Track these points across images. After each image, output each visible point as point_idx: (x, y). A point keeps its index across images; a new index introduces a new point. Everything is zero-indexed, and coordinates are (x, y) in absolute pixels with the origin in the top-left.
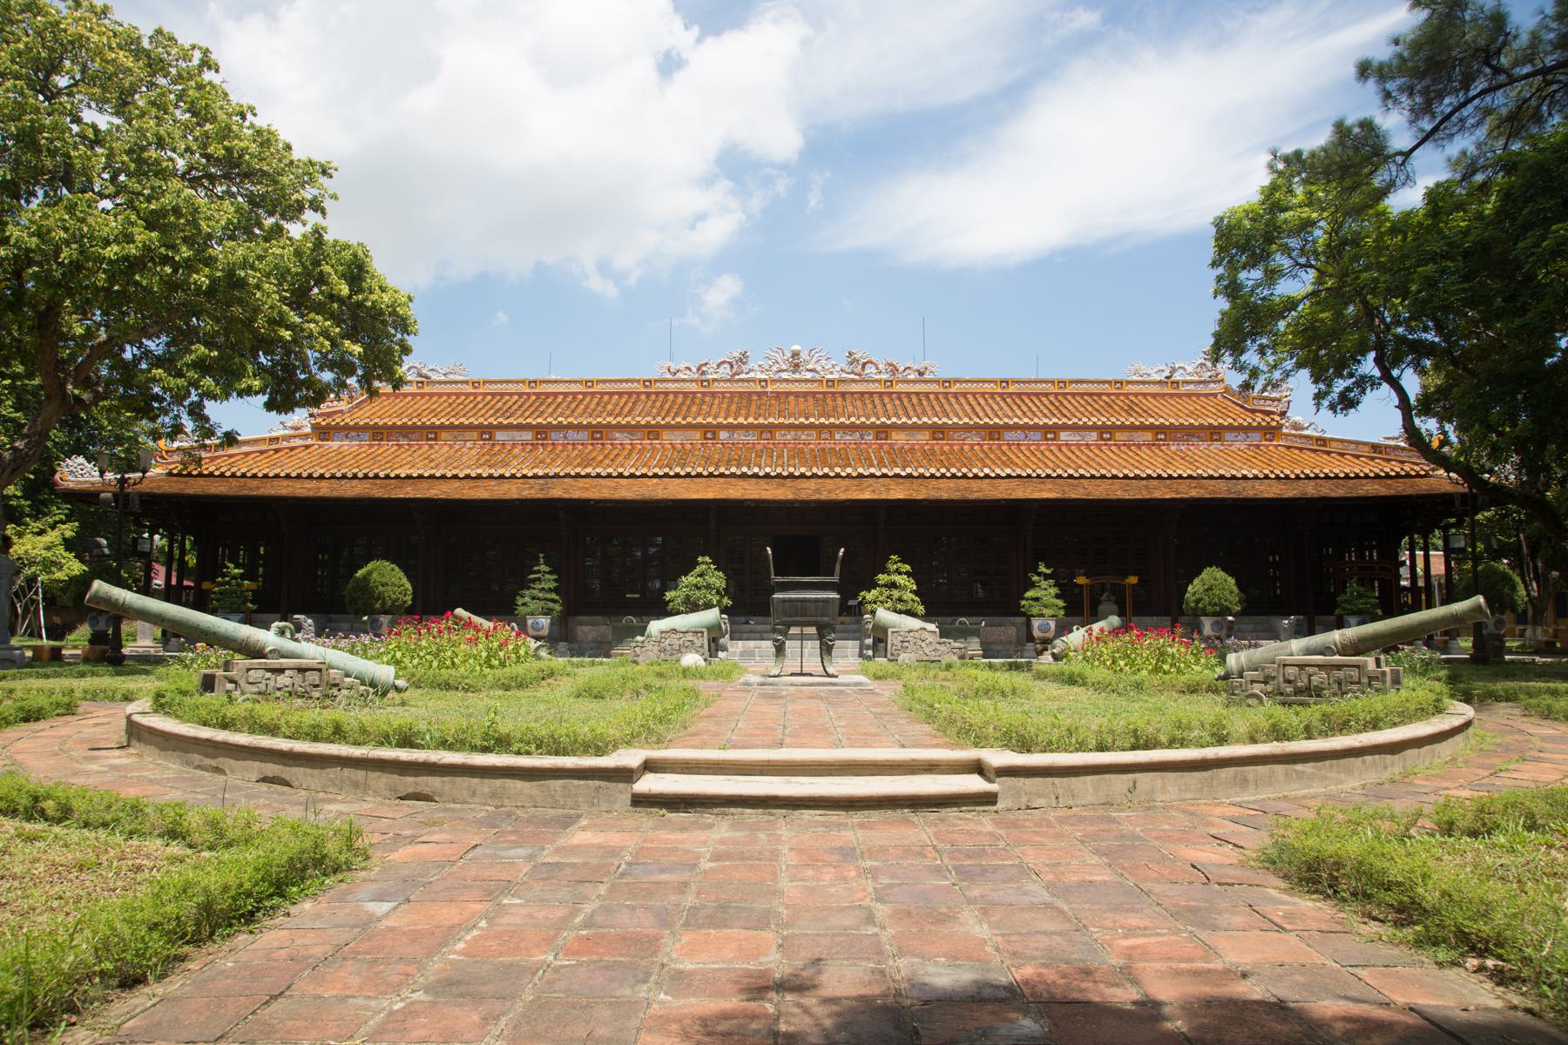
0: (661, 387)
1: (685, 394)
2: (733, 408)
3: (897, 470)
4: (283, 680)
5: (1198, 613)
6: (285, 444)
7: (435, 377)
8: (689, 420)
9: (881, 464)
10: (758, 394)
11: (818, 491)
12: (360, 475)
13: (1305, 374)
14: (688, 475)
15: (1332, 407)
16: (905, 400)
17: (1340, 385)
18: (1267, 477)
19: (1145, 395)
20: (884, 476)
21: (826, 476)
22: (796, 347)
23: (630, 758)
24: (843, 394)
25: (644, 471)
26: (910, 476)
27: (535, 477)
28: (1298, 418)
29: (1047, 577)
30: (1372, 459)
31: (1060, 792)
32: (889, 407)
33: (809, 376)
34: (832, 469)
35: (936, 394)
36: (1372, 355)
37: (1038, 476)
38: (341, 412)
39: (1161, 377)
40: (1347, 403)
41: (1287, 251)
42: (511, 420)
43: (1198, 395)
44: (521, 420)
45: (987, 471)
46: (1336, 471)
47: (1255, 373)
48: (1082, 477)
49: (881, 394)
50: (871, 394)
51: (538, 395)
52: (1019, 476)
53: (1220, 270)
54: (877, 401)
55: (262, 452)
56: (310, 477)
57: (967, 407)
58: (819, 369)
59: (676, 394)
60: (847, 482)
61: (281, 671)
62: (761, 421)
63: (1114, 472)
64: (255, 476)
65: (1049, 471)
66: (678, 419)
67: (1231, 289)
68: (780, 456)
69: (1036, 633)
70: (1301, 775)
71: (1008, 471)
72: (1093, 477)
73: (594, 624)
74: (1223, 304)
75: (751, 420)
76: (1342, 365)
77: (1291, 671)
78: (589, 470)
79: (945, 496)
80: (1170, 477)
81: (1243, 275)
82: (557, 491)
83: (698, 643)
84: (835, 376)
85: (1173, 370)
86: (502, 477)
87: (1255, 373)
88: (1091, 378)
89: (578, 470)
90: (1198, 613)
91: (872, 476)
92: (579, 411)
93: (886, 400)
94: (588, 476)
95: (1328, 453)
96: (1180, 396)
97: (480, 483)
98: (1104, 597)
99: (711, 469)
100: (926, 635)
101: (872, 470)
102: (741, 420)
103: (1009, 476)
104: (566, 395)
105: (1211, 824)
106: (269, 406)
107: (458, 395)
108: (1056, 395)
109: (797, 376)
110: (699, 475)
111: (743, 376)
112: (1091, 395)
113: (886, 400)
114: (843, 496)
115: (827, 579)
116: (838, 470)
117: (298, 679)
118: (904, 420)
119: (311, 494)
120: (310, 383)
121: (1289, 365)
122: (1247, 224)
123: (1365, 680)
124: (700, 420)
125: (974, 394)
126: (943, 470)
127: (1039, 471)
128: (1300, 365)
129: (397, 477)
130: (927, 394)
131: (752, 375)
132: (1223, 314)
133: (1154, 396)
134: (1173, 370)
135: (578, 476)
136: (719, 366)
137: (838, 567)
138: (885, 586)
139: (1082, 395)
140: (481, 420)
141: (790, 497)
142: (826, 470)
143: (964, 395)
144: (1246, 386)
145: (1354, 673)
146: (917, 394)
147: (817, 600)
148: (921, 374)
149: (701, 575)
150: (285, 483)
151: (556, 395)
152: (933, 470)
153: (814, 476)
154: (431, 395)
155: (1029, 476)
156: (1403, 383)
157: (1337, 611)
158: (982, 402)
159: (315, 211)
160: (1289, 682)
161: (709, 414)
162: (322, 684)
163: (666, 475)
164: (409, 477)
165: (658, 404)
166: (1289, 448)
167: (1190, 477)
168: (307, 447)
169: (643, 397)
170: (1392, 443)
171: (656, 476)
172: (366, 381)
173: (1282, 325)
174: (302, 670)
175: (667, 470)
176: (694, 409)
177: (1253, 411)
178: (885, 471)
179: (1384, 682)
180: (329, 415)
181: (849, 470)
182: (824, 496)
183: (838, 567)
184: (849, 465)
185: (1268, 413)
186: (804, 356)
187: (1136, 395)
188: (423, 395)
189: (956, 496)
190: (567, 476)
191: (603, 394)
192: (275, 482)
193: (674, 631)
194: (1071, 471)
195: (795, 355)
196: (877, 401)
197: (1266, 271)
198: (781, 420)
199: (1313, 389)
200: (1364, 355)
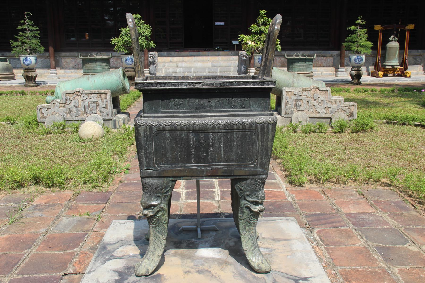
29: (362, 27)
83: (102, 104)
98: (391, 39)
100: (318, 94)
138: (256, 33)
147: (229, 129)
193: (78, 93)
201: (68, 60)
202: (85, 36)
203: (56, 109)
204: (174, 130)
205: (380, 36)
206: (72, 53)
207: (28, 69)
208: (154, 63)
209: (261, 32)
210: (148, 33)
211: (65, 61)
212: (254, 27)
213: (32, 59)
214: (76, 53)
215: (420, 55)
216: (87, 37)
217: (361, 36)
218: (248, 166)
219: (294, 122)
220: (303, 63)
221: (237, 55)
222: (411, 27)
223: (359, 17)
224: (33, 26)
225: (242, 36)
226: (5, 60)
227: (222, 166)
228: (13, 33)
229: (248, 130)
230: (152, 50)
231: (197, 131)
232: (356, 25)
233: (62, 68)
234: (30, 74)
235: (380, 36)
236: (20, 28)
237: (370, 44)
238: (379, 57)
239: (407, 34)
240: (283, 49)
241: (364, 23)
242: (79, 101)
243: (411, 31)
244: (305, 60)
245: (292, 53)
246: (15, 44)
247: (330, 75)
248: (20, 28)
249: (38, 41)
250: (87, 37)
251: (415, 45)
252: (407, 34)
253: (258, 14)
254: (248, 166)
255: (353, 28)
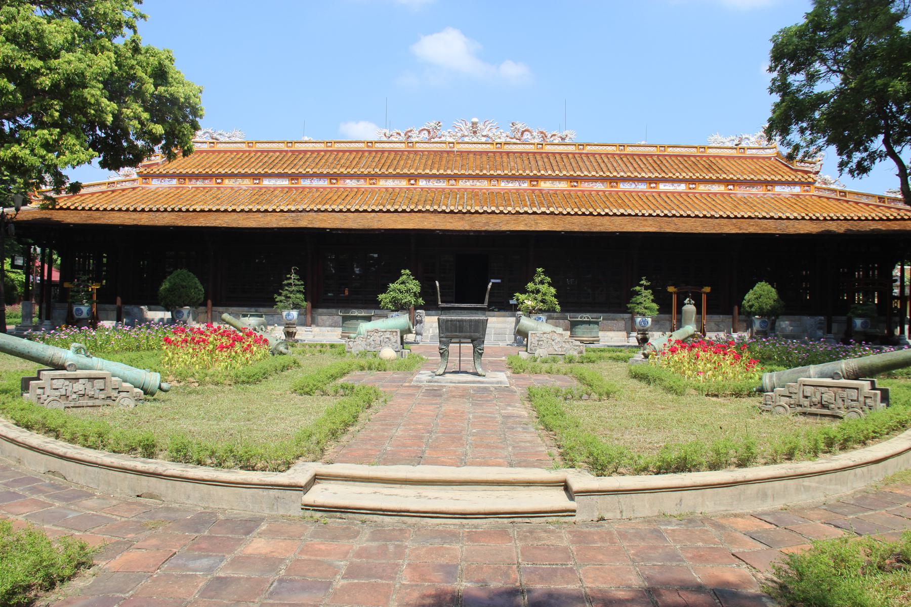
0: (379, 146)
1: (396, 152)
2: (430, 162)
3: (543, 209)
4: (79, 386)
5: (750, 314)
6: (119, 186)
7: (222, 139)
8: (398, 171)
9: (532, 204)
10: (448, 152)
11: (487, 223)
12: (169, 209)
13: (833, 148)
14: (396, 211)
15: (851, 172)
16: (551, 158)
17: (857, 156)
18: (803, 218)
19: (720, 157)
20: (534, 213)
21: (493, 212)
22: (475, 120)
23: (300, 474)
24: (508, 153)
25: (365, 208)
26: (552, 213)
27: (289, 211)
28: (827, 177)
29: (646, 288)
30: (878, 206)
31: (624, 508)
32: (540, 163)
33: (484, 140)
34: (497, 207)
35: (574, 154)
36: (881, 137)
37: (643, 215)
38: (157, 164)
39: (732, 145)
40: (862, 169)
41: (823, 60)
42: (274, 170)
43: (758, 158)
44: (281, 171)
45: (607, 211)
46: (852, 215)
47: (797, 148)
48: (674, 216)
49: (534, 153)
50: (528, 153)
51: (293, 152)
52: (630, 215)
53: (775, 74)
54: (531, 158)
55: (103, 192)
56: (135, 210)
57: (595, 164)
58: (491, 135)
59: (390, 152)
60: (508, 217)
61: (77, 379)
62: (449, 172)
63: (697, 213)
64: (98, 209)
65: (651, 212)
66: (390, 171)
67: (782, 87)
68: (462, 198)
69: (638, 326)
70: (807, 489)
71: (622, 211)
72: (681, 216)
73: (330, 315)
74: (776, 98)
75: (441, 172)
76: (860, 145)
77: (809, 391)
78: (327, 207)
79: (577, 229)
80: (736, 217)
81: (791, 78)
82: (304, 222)
83: (393, 339)
84: (503, 140)
85: (741, 140)
86: (266, 211)
87: (797, 148)
88: (683, 144)
89: (319, 207)
90: (750, 314)
91: (526, 213)
92: (321, 164)
93: (538, 157)
94: (326, 211)
95: (847, 202)
96: (746, 158)
97: (251, 215)
98: (686, 301)
99: (412, 207)
100: (555, 336)
101: (526, 209)
102: (435, 171)
103: (622, 215)
104: (312, 152)
105: (733, 541)
106: (103, 165)
107: (238, 152)
108: (658, 156)
109: (475, 140)
110: (404, 211)
111: (436, 140)
112: (682, 156)
113: (538, 157)
114: (504, 228)
115: (479, 306)
116: (501, 208)
117: (89, 385)
118: (550, 172)
119: (135, 223)
120: (132, 147)
121: (821, 141)
122: (795, 40)
123: (861, 399)
124: (405, 171)
125: (600, 154)
126: (576, 210)
127: (644, 212)
128: (829, 142)
129: (194, 211)
130: (567, 154)
131: (443, 139)
132: (777, 105)
133: (727, 158)
134: (741, 140)
135: (319, 211)
136: (420, 132)
137: (487, 297)
138: (533, 292)
139: (676, 156)
140: (253, 170)
141: (467, 228)
142: (493, 208)
143: (593, 154)
144: (790, 157)
145: (854, 394)
146: (560, 154)
147: (471, 321)
148: (563, 139)
149: (403, 283)
150: (118, 214)
151: (305, 152)
152: (569, 210)
153: (485, 212)
154: (219, 152)
155: (636, 215)
156: (902, 157)
157: (849, 314)
158: (606, 160)
159: (130, 28)
160: (806, 397)
161: (411, 167)
162: (105, 392)
163: (381, 211)
164: (202, 211)
165: (377, 159)
166: (820, 197)
167: (750, 217)
168: (134, 189)
169: (366, 154)
170: (893, 195)
171: (373, 211)
172: (166, 149)
173: (817, 115)
174: (91, 379)
175: (381, 207)
176: (402, 163)
177: (796, 171)
178: (535, 209)
179: (875, 401)
180: (149, 166)
181: (510, 209)
182: (491, 228)
183: (487, 297)
184: (510, 205)
185: (806, 172)
186: (480, 126)
187: (714, 157)
188: (213, 152)
189: (585, 229)
190: (312, 210)
191: (338, 151)
192: (112, 214)
193: (377, 331)
194: (666, 212)
195: (474, 124)
196: (531, 158)
197: (807, 75)
198: (463, 172)
199: (838, 159)
200: (876, 136)
201: (325, 318)
202: (116, 299)
203: (359, 342)
204: (452, 321)
205: (674, 297)
206: (330, 310)
207: (288, 325)
208: (421, 322)
209: (538, 291)
210: (417, 289)
211: (320, 319)
212: (530, 286)
213: (294, 314)
214: (334, 311)
215: (722, 321)
216: (347, 293)
217: (645, 298)
218: (477, 335)
219: (536, 355)
220: (587, 326)
221: (514, 316)
222: (707, 289)
223: (644, 278)
224: (298, 280)
225: (517, 294)
226: (261, 316)
227: (468, 334)
228: (278, 287)
229: (478, 321)
230: (421, 307)
231: (459, 321)
232: (641, 285)
233: (318, 326)
234: (291, 330)
235: (674, 297)
236: (285, 282)
237: (655, 306)
238: (675, 322)
239: (704, 297)
240: (562, 311)
241: (649, 284)
242: (376, 337)
243: (707, 294)
244: (589, 323)
245: (577, 315)
246: (279, 298)
247: (621, 341)
248: (285, 282)
249: (302, 296)
250: (347, 293)
251: (713, 309)
252: (704, 297)
253: (535, 272)
254: (477, 335)
255: (638, 288)
